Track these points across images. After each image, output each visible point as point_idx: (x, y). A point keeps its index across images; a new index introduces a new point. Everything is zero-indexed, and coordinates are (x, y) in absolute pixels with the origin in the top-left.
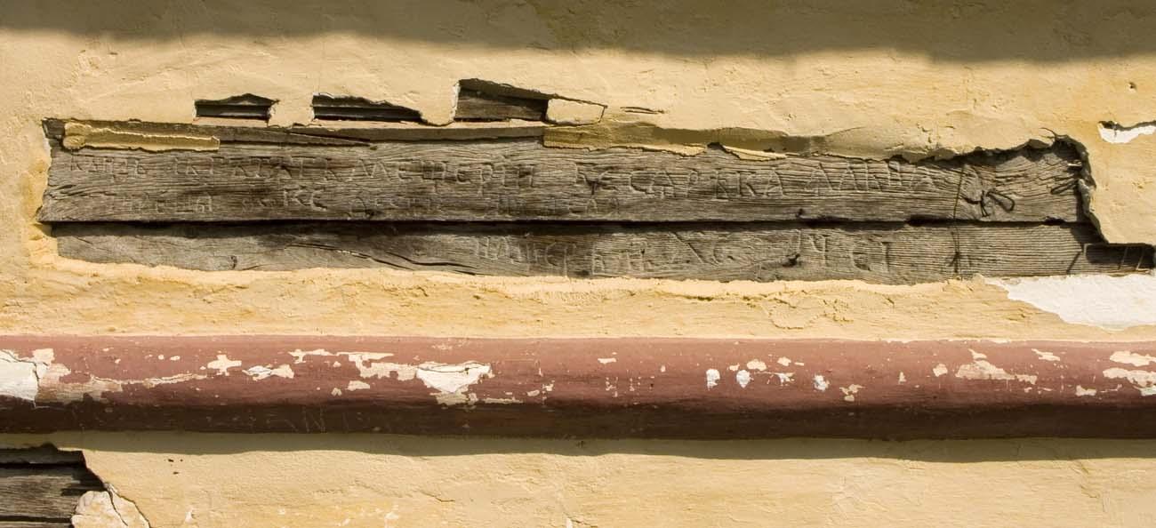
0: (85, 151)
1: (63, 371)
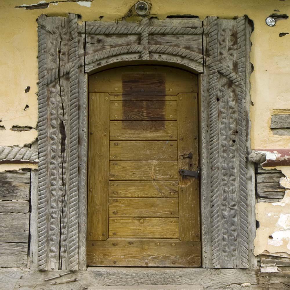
0: (278, 115)
1: (280, 155)
